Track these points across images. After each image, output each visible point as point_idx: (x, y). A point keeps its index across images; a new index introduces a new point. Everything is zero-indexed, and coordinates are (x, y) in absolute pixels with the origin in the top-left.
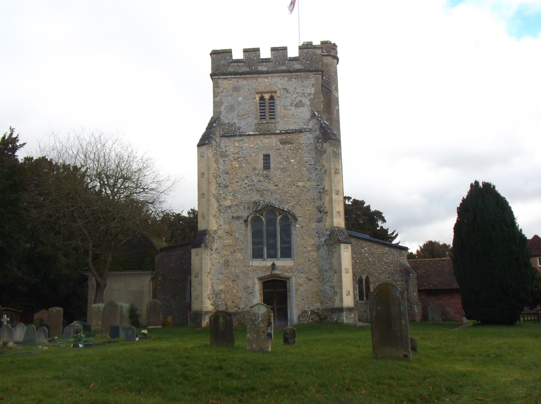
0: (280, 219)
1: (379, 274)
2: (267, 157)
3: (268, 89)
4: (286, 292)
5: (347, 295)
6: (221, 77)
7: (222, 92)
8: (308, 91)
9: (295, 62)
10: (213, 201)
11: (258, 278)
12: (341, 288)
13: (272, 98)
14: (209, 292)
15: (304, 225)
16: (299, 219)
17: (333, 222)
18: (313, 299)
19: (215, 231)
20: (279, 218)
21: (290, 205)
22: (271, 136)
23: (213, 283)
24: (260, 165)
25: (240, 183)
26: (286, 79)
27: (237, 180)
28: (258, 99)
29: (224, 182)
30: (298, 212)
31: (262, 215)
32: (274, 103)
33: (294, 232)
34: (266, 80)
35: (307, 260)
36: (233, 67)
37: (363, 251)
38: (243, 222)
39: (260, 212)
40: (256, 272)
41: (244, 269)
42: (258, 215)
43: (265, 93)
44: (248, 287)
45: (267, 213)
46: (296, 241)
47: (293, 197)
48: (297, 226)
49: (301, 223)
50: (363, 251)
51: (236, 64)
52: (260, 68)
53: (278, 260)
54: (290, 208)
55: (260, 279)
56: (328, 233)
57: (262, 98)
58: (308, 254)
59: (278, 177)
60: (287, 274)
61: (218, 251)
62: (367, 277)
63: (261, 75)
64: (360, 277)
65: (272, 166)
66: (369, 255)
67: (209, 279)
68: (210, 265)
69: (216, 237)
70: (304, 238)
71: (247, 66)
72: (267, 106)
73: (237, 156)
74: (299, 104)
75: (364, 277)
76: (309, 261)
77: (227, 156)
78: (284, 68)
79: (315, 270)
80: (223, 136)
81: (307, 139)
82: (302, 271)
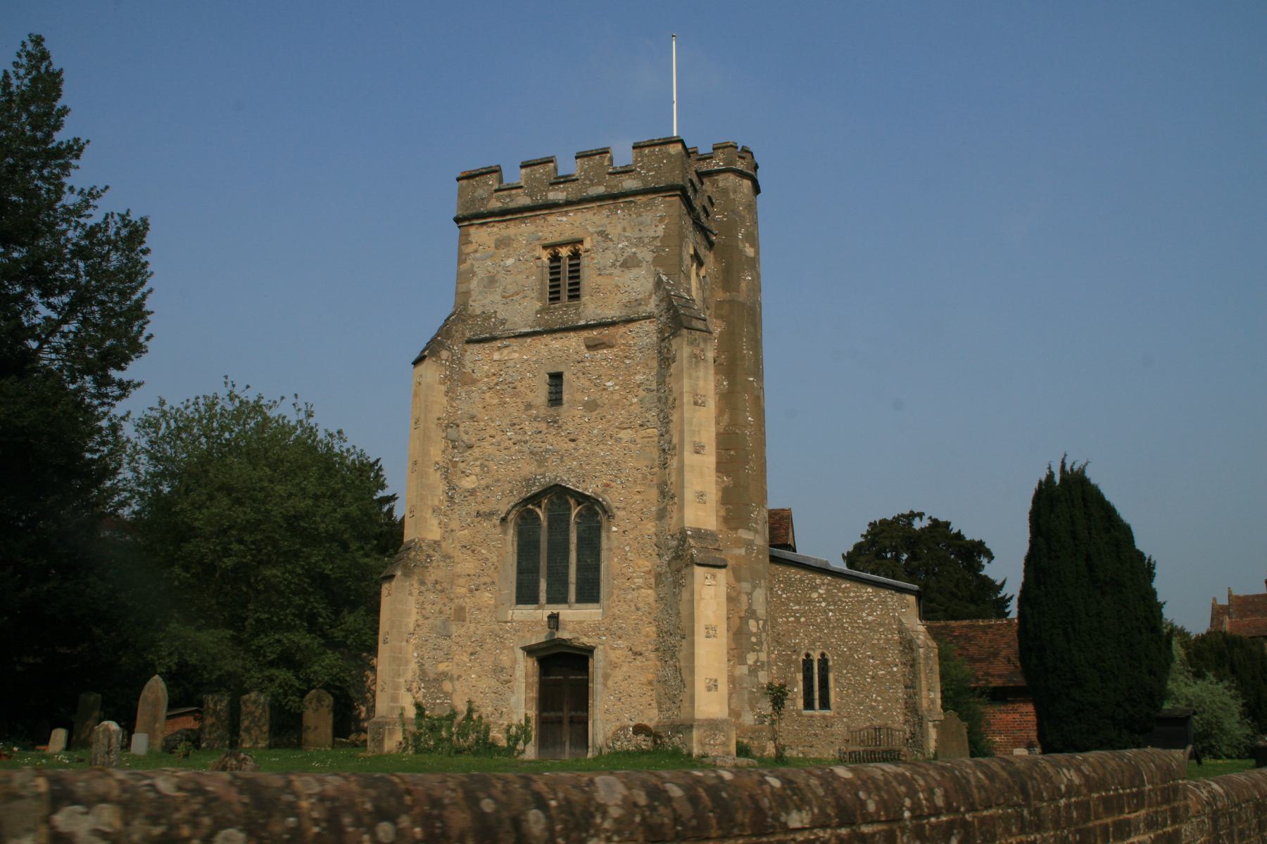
0: (579, 515)
1: (850, 649)
2: (556, 378)
3: (567, 236)
4: (587, 681)
5: (709, 689)
7: (476, 251)
8: (651, 234)
9: (625, 177)
10: (436, 478)
11: (524, 649)
12: (692, 671)
13: (576, 255)
14: (409, 676)
15: (629, 526)
16: (621, 514)
17: (682, 519)
18: (643, 700)
19: (435, 542)
20: (574, 513)
23: (421, 657)
24: (541, 394)
25: (498, 438)
27: (493, 432)
29: (465, 437)
30: (612, 499)
31: (540, 507)
32: (578, 265)
33: (604, 543)
35: (633, 608)
36: (498, 199)
37: (815, 595)
38: (498, 522)
39: (535, 499)
40: (520, 634)
41: (496, 627)
42: (530, 506)
44: (502, 669)
45: (551, 502)
46: (610, 565)
48: (614, 529)
49: (622, 523)
50: (815, 595)
51: (505, 193)
52: (553, 196)
53: (570, 608)
54: (599, 490)
55: (530, 651)
56: (675, 543)
57: (555, 258)
58: (635, 593)
59: (577, 420)
60: (585, 640)
62: (823, 655)
64: (808, 655)
65: (565, 397)
66: (828, 604)
67: (411, 648)
69: (436, 557)
70: (627, 556)
71: (526, 195)
72: (564, 276)
74: (628, 263)
75: (816, 656)
76: (638, 609)
77: (474, 382)
78: (601, 190)
79: (652, 630)
80: (469, 342)
81: (646, 334)
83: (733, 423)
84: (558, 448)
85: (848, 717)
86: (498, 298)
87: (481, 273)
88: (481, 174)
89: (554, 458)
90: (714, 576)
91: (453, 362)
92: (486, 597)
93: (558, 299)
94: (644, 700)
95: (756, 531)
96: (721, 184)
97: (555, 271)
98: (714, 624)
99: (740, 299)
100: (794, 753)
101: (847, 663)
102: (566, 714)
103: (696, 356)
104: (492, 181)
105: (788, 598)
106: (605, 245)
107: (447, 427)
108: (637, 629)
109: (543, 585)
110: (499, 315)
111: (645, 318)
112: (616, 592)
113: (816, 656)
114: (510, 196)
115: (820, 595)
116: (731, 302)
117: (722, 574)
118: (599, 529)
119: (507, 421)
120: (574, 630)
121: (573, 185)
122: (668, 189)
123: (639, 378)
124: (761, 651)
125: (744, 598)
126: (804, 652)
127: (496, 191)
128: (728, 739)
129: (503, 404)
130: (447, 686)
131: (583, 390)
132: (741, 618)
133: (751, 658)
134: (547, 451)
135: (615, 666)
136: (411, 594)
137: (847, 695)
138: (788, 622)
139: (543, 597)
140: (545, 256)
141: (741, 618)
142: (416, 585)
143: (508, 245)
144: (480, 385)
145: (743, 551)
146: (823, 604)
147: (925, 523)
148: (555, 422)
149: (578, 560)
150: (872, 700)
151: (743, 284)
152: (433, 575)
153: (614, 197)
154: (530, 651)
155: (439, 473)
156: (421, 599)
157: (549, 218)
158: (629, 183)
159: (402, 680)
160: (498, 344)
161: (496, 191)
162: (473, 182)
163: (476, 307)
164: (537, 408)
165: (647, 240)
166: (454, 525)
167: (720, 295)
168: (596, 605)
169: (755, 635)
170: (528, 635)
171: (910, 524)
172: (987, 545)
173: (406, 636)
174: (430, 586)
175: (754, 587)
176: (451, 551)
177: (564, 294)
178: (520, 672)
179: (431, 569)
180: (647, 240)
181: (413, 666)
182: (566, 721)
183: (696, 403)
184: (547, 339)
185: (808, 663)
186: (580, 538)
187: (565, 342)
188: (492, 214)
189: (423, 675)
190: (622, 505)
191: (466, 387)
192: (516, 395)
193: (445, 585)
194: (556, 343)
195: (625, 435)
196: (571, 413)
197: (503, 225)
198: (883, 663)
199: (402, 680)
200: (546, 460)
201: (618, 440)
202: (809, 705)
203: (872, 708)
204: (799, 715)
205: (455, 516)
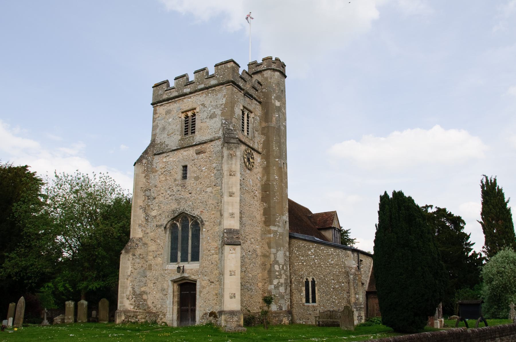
1: (324, 276)
2: (185, 167)
3: (190, 107)
5: (231, 298)
6: (158, 104)
8: (221, 103)
9: (211, 79)
11: (172, 281)
13: (194, 115)
14: (128, 293)
16: (206, 223)
19: (140, 238)
21: (199, 210)
22: (189, 148)
24: (179, 175)
25: (164, 194)
26: (204, 95)
27: (162, 192)
28: (183, 118)
34: (190, 100)
36: (166, 94)
37: (310, 253)
38: (163, 229)
39: (175, 218)
42: (175, 222)
43: (188, 111)
46: (203, 245)
47: (202, 203)
50: (310, 253)
54: (199, 214)
57: (187, 117)
60: (193, 277)
61: (141, 256)
62: (313, 279)
63: (186, 97)
64: (307, 279)
65: (188, 175)
66: (315, 257)
67: (129, 282)
68: (130, 269)
70: (208, 241)
71: (176, 91)
72: (189, 125)
73: (164, 170)
75: (310, 280)
76: (212, 263)
77: (156, 171)
78: (202, 86)
80: (155, 155)
82: (205, 273)
83: (268, 180)
84: (185, 197)
85: (323, 306)
86: (166, 135)
87: (160, 126)
88: (161, 84)
89: (183, 201)
90: (234, 249)
91: (148, 164)
92: (159, 260)
93: (187, 134)
94: (215, 301)
95: (279, 226)
96: (265, 76)
97: (186, 122)
98: (234, 270)
99: (273, 125)
100: (301, 322)
101: (323, 282)
102: (189, 308)
103: (231, 155)
104: (164, 87)
105: (299, 254)
106: (204, 109)
107: (145, 191)
108: (212, 272)
109: (179, 254)
110: (166, 143)
111: (217, 139)
112: (204, 256)
113: (310, 280)
114: (170, 92)
115: (312, 252)
116: (268, 127)
117: (238, 248)
118: (199, 230)
119: (168, 187)
120: (189, 273)
121: (193, 85)
122: (228, 82)
123: (214, 165)
124: (281, 278)
125: (272, 256)
126: (305, 278)
127: (166, 91)
128: (240, 319)
129: (166, 180)
130: (145, 297)
131: (194, 172)
132: (271, 264)
133: (275, 282)
134: (181, 198)
135: (204, 288)
136: (129, 260)
137: (323, 297)
138: (299, 265)
139: (179, 259)
140: (183, 116)
141: (271, 264)
142: (131, 256)
143: (170, 113)
144: (158, 172)
145: (272, 235)
146: (313, 257)
147: (434, 210)
148: (184, 186)
149: (192, 243)
150: (333, 299)
151: (274, 119)
152: (138, 252)
153: (207, 88)
154: (174, 281)
155: (142, 210)
156: (133, 262)
157: (184, 100)
158: (213, 82)
159: (125, 295)
160: (165, 155)
161: (166, 91)
162: (158, 88)
163: (158, 141)
164: (178, 180)
165: (219, 106)
166: (148, 231)
167: (264, 124)
168: (198, 262)
169: (278, 271)
170: (173, 275)
171: (426, 211)
172: (462, 218)
173: (126, 277)
174: (137, 256)
175: (277, 251)
176: (147, 242)
177: (190, 132)
178: (170, 291)
179: (138, 249)
180: (219, 106)
181: (130, 289)
182: (190, 310)
183: (230, 175)
184: (182, 151)
185: (307, 282)
186: (192, 234)
187: (188, 152)
188: (164, 101)
189: (134, 293)
190: (207, 220)
191: (154, 174)
192: (171, 176)
193: (144, 255)
194: (184, 153)
195: (209, 190)
196: (190, 181)
197: (168, 105)
198: (338, 282)
199: (125, 295)
200: (180, 202)
201: (206, 192)
202: (307, 301)
203: (333, 302)
204: (304, 305)
205: (149, 227)
